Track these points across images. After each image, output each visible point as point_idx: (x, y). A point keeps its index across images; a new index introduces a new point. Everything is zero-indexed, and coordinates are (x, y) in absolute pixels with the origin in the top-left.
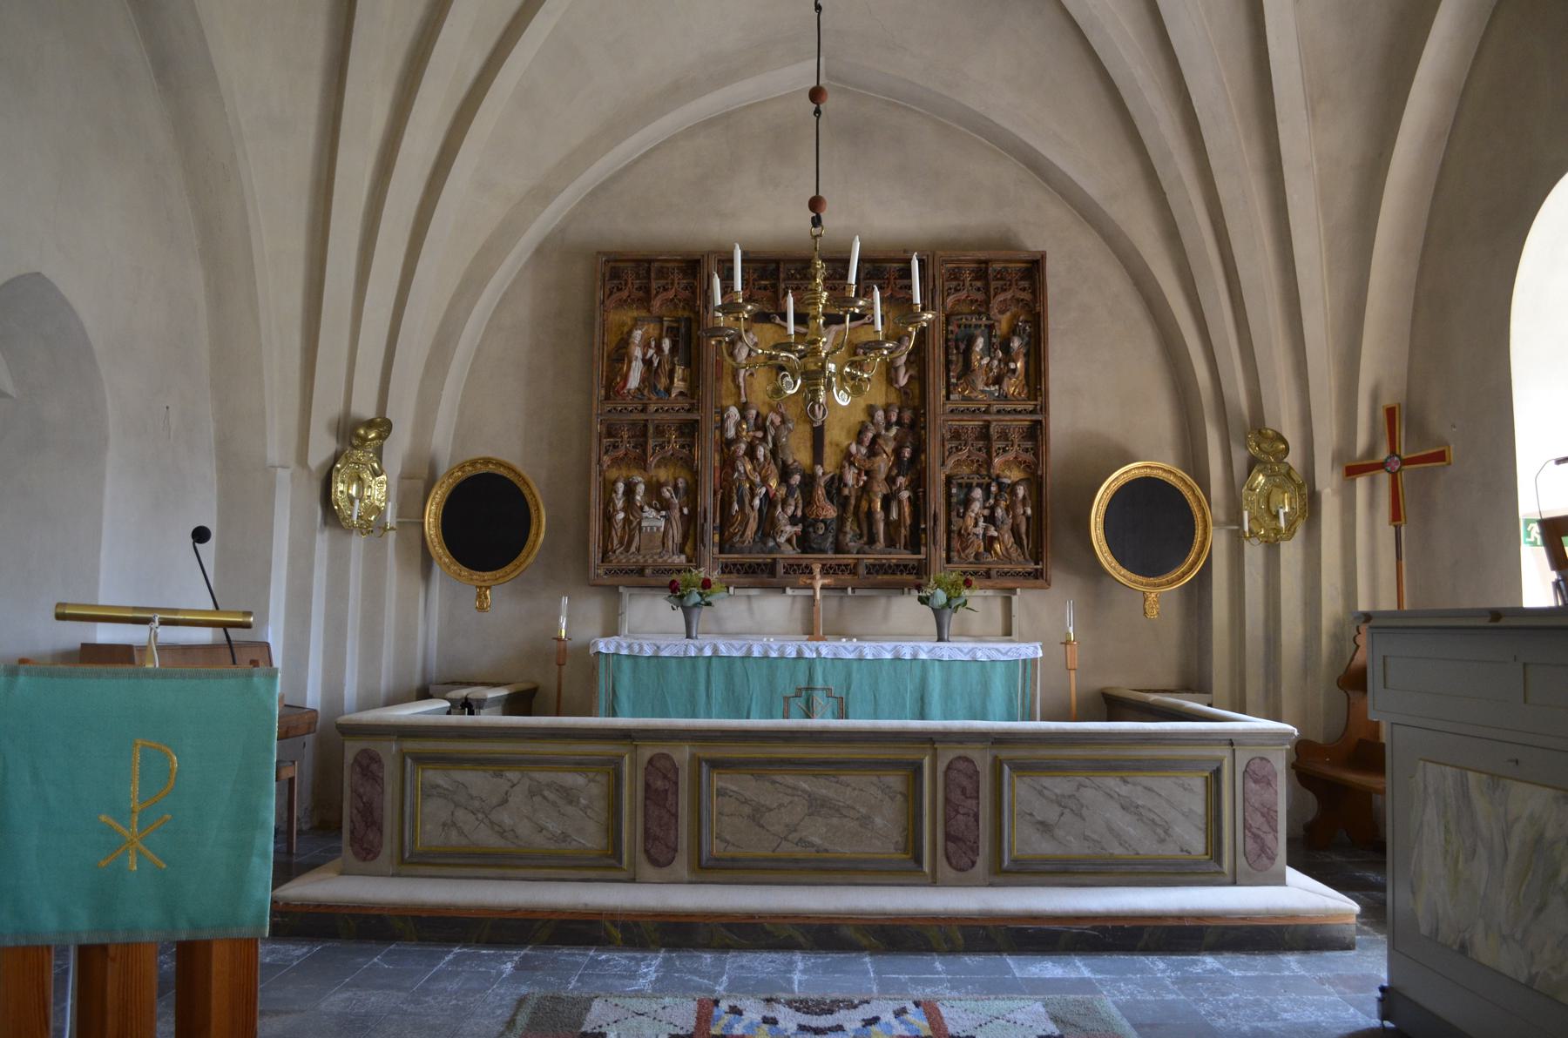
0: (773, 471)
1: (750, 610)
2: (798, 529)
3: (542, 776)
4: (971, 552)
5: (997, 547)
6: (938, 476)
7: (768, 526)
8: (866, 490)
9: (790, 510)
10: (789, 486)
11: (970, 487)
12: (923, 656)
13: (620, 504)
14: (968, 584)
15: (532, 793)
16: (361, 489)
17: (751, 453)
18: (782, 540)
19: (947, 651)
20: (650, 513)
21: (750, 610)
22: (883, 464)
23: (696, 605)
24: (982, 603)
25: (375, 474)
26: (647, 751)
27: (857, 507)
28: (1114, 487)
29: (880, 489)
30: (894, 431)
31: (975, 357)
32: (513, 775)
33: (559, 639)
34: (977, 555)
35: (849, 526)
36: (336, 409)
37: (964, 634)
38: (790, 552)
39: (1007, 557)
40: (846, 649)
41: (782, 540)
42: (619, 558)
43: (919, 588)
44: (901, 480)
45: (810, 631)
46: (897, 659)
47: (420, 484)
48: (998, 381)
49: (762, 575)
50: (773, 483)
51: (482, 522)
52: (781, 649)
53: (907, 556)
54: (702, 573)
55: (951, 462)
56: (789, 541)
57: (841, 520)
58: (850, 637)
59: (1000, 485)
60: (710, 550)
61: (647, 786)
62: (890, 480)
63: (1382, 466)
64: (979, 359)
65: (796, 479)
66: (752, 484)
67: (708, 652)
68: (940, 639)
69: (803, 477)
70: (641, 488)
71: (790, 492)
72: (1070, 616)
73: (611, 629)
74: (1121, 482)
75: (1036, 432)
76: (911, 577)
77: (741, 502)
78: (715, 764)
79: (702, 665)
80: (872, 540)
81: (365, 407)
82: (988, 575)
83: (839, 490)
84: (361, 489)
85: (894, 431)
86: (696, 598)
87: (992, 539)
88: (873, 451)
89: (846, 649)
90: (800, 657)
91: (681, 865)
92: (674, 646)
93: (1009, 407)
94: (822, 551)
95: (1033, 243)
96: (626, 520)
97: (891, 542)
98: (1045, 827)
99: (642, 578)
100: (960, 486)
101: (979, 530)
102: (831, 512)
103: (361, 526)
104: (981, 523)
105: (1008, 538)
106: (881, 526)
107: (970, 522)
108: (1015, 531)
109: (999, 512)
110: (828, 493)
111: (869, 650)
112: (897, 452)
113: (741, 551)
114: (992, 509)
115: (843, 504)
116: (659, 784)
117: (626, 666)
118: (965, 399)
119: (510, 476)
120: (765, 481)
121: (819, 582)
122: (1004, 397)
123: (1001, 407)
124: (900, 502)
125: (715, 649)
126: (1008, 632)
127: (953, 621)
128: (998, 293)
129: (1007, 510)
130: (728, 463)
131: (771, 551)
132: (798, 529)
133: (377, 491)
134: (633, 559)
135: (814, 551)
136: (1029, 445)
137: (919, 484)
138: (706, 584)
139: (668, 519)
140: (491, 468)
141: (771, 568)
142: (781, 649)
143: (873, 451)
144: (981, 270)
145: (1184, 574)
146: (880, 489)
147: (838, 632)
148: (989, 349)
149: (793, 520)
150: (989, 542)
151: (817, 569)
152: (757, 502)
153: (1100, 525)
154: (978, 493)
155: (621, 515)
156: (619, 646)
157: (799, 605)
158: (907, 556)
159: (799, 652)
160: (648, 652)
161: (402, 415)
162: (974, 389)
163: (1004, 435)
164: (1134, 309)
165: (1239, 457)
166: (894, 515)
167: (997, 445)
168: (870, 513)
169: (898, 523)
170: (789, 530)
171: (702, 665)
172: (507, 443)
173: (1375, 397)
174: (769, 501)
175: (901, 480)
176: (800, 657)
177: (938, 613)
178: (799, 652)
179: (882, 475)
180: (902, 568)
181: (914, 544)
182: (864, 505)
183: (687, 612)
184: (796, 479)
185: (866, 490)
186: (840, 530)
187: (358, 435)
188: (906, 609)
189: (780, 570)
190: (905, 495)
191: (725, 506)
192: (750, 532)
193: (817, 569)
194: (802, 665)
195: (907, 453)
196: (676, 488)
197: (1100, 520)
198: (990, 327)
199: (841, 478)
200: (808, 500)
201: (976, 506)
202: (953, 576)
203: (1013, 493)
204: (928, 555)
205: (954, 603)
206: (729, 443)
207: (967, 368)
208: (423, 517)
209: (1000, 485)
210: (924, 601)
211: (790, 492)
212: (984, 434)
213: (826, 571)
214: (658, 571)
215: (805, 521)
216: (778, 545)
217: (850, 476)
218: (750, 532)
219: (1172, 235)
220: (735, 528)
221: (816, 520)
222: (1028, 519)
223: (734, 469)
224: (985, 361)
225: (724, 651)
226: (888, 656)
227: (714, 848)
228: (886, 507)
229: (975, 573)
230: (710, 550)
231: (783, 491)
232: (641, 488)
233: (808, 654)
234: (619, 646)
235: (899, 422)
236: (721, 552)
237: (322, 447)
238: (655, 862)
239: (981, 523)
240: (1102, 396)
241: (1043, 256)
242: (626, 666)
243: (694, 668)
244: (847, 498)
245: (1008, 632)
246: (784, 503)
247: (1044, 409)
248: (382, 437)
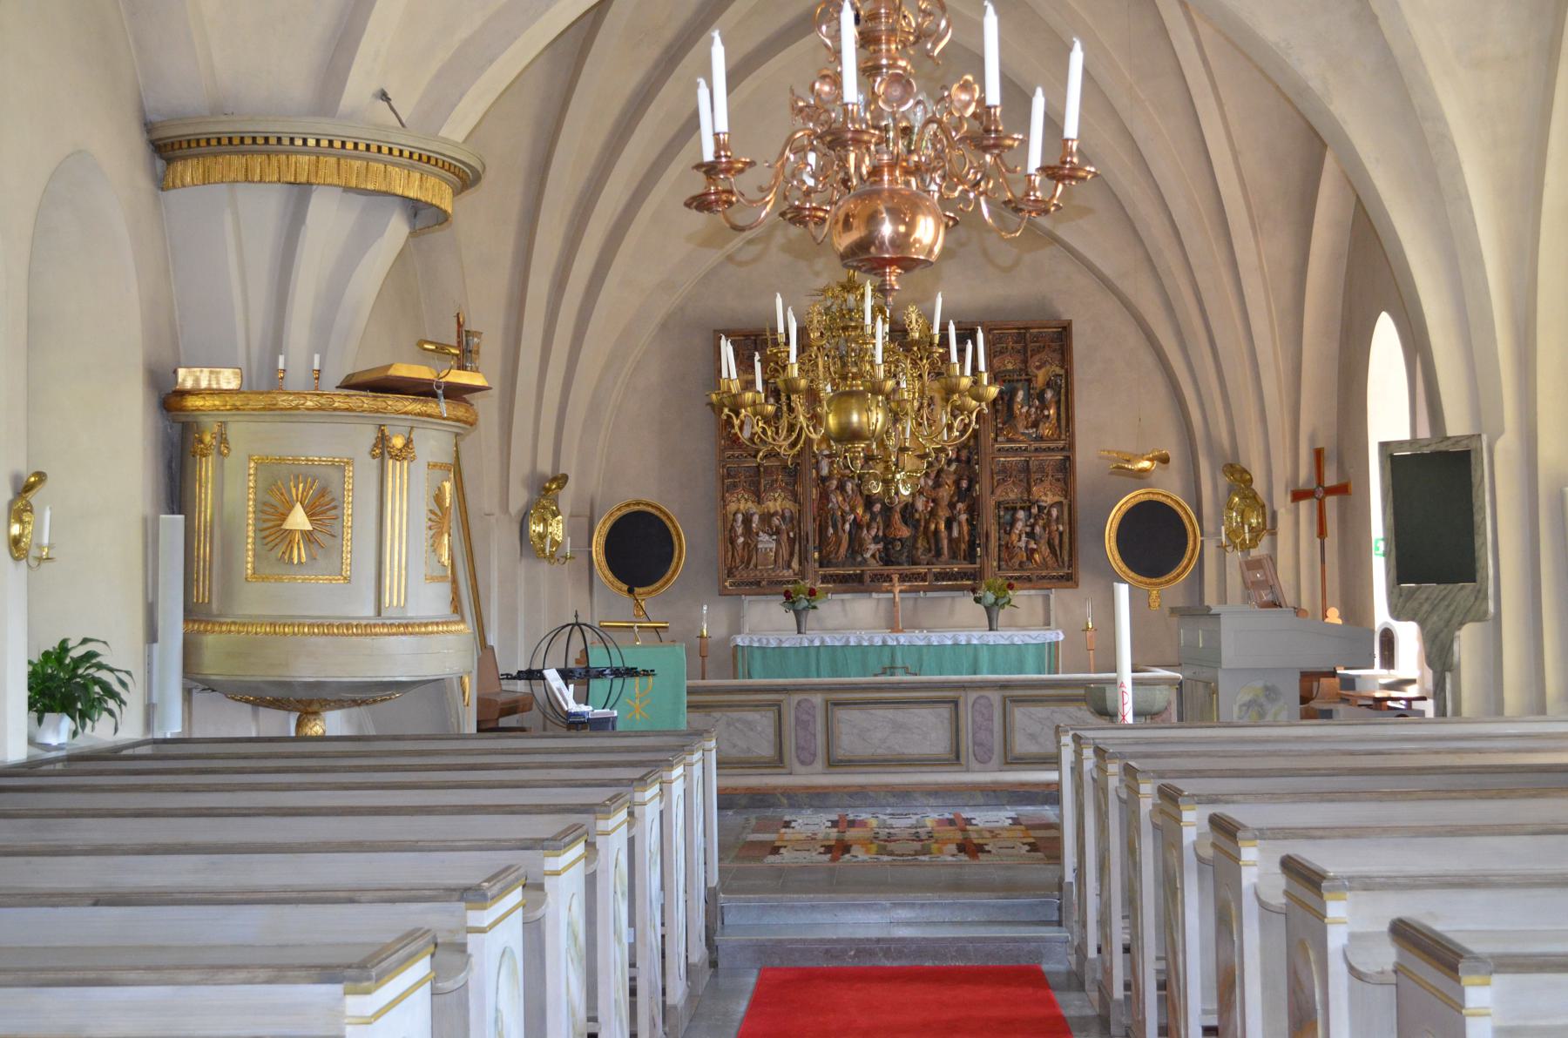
0: (860, 501)
1: (844, 610)
2: (880, 546)
3: (735, 715)
4: (1016, 561)
5: (1037, 556)
6: (989, 503)
7: (856, 546)
8: (933, 513)
9: (873, 532)
10: (872, 513)
11: (1014, 510)
12: (975, 642)
13: (740, 531)
14: (1011, 587)
15: (728, 724)
16: (546, 527)
17: (841, 487)
18: (868, 555)
19: (992, 638)
20: (764, 537)
21: (844, 610)
22: (945, 493)
23: (805, 609)
24: (1024, 599)
25: (555, 515)
26: (796, 698)
27: (926, 527)
28: (1124, 509)
29: (944, 513)
30: (953, 467)
31: (1017, 407)
32: (717, 715)
33: (702, 637)
34: (1021, 564)
35: (921, 543)
36: (526, 469)
37: (1012, 625)
38: (874, 566)
39: (1044, 565)
40: (918, 638)
41: (868, 555)
42: (742, 574)
43: (974, 590)
44: (960, 506)
45: (893, 628)
46: (956, 645)
47: (585, 521)
48: (1035, 425)
49: (855, 583)
50: (860, 511)
51: (638, 549)
52: (871, 639)
53: (966, 566)
54: (808, 584)
55: (998, 491)
56: (873, 556)
57: (915, 538)
58: (921, 629)
59: (1040, 509)
60: (813, 566)
61: (797, 718)
62: (952, 506)
63: (1331, 491)
64: (1020, 408)
65: (877, 507)
66: (843, 511)
67: (817, 643)
68: (991, 629)
69: (883, 504)
70: (756, 518)
71: (873, 518)
72: (1089, 610)
73: (736, 628)
74: (1129, 505)
75: (1066, 468)
76: (971, 581)
77: (835, 527)
78: (837, 704)
79: (813, 653)
80: (939, 553)
81: (545, 467)
82: (1029, 579)
83: (912, 515)
84: (546, 527)
85: (953, 467)
86: (805, 603)
87: (1033, 551)
88: (938, 484)
89: (918, 638)
90: (884, 645)
91: (819, 765)
92: (791, 640)
93: (1044, 445)
94: (899, 564)
95: (1067, 310)
96: (745, 544)
97: (954, 555)
98: (1032, 737)
99: (759, 587)
100: (1006, 509)
101: (1022, 544)
102: (905, 532)
103: (552, 555)
104: (1024, 538)
105: (1045, 550)
106: (945, 542)
107: (1014, 537)
108: (1050, 544)
109: (1038, 529)
110: (903, 517)
111: (935, 639)
112: (957, 483)
113: (836, 565)
114: (1033, 526)
115: (915, 525)
116: (805, 717)
117: (757, 654)
118: (1010, 440)
119: (657, 513)
120: (853, 510)
121: (897, 590)
122: (1040, 438)
123: (1037, 445)
124: (960, 524)
125: (823, 641)
126: (1047, 623)
127: (1002, 615)
128: (1035, 352)
129: (1044, 528)
130: (824, 497)
131: (860, 564)
132: (880, 546)
133: (557, 529)
134: (752, 575)
135: (893, 564)
136: (1060, 476)
137: (973, 511)
138: (812, 592)
139: (778, 542)
140: (642, 508)
141: (859, 578)
142: (871, 639)
143: (938, 484)
144: (1022, 334)
145: (1182, 574)
146: (944, 513)
147: (913, 626)
148: (1028, 396)
149: (876, 539)
150: (1031, 553)
151: (896, 578)
152: (847, 527)
153: (1113, 540)
154: (1021, 514)
155: (741, 540)
156: (752, 640)
157: (883, 606)
158: (966, 566)
159: (884, 641)
160: (773, 644)
161: (569, 466)
162: (1016, 432)
163: (1041, 469)
164: (1148, 360)
165: (1222, 490)
166: (955, 534)
167: (1034, 476)
168: (937, 531)
169: (958, 540)
170: (873, 547)
171: (813, 653)
172: (642, 486)
173: (1312, 438)
174: (857, 524)
175: (960, 506)
176: (884, 645)
177: (988, 609)
178: (884, 641)
179: (945, 503)
180: (963, 575)
181: (971, 556)
182: (933, 527)
183: (798, 614)
184: (877, 507)
185: (933, 513)
186: (914, 547)
187: (546, 490)
188: (965, 607)
189: (867, 579)
190: (964, 517)
191: (822, 531)
192: (843, 550)
193: (896, 578)
194: (887, 652)
195: (964, 484)
196: (783, 517)
197: (1113, 535)
198: (1029, 381)
199: (913, 505)
200: (888, 524)
201: (1019, 525)
202: (1000, 581)
203: (1049, 514)
204: (982, 563)
205: (1001, 602)
206: (824, 480)
207: (1011, 415)
208: (590, 545)
209: (1040, 509)
210: (977, 600)
211: (873, 518)
212: (1026, 469)
213: (903, 579)
214: (771, 583)
215: (887, 541)
216: (865, 560)
217: (920, 505)
218: (843, 550)
219: (1169, 307)
220: (831, 548)
221: (895, 539)
222: (1061, 534)
223: (828, 500)
224: (1024, 410)
225: (829, 642)
226: (949, 642)
227: (840, 753)
228: (949, 527)
229: (1017, 578)
230: (813, 566)
231: (868, 517)
232: (756, 518)
233: (890, 642)
234: (752, 640)
235: (958, 459)
236: (821, 566)
237: (519, 497)
238: (803, 763)
239: (1024, 538)
240: (1117, 431)
241: (1070, 323)
242: (757, 654)
243: (807, 655)
244: (918, 521)
245: (1047, 623)
246: (869, 527)
247: (1070, 447)
248: (560, 487)
